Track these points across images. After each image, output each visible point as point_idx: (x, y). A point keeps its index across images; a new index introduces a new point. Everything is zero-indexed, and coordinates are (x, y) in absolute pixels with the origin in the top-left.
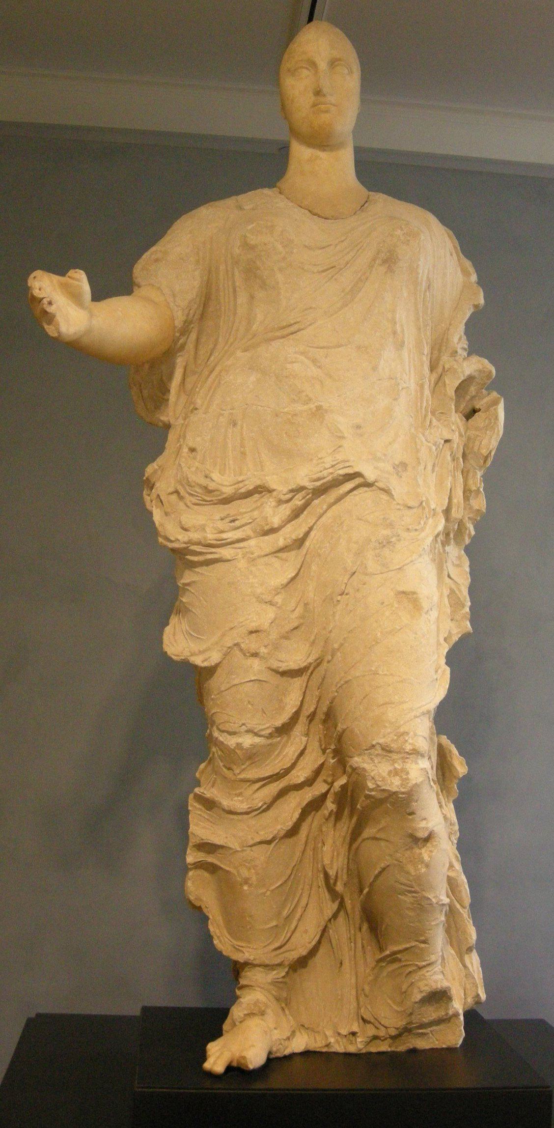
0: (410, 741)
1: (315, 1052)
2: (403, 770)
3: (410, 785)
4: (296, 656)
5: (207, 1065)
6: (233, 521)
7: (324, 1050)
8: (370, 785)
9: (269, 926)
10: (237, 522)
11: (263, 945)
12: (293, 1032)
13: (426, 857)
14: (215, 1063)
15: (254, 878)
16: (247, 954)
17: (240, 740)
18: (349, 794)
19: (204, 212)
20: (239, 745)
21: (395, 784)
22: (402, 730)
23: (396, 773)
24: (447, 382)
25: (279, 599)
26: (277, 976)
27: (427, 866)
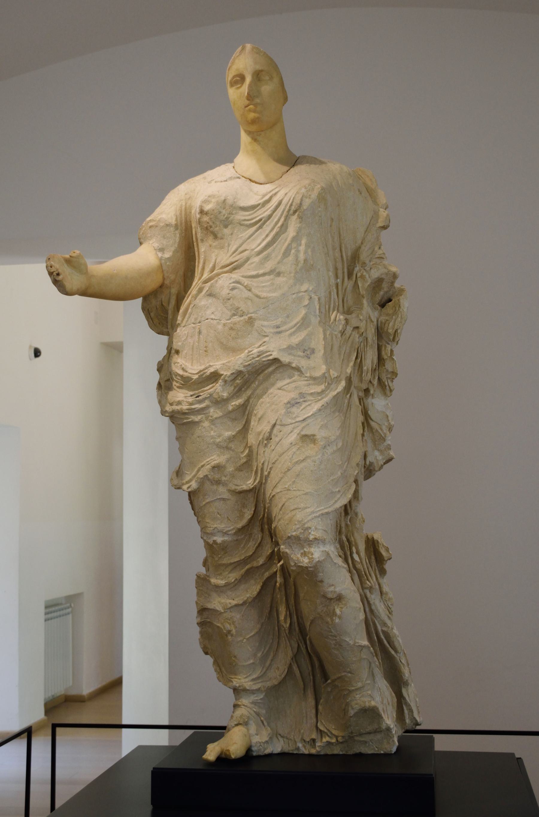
0: (313, 533)
2: (309, 552)
3: (314, 562)
4: (249, 483)
5: (204, 757)
7: (295, 752)
8: (293, 564)
10: (200, 398)
11: (245, 676)
12: (271, 738)
13: (338, 611)
14: (210, 754)
17: (215, 538)
20: (215, 542)
21: (305, 562)
22: (306, 526)
23: (304, 554)
25: (232, 445)
26: (256, 698)
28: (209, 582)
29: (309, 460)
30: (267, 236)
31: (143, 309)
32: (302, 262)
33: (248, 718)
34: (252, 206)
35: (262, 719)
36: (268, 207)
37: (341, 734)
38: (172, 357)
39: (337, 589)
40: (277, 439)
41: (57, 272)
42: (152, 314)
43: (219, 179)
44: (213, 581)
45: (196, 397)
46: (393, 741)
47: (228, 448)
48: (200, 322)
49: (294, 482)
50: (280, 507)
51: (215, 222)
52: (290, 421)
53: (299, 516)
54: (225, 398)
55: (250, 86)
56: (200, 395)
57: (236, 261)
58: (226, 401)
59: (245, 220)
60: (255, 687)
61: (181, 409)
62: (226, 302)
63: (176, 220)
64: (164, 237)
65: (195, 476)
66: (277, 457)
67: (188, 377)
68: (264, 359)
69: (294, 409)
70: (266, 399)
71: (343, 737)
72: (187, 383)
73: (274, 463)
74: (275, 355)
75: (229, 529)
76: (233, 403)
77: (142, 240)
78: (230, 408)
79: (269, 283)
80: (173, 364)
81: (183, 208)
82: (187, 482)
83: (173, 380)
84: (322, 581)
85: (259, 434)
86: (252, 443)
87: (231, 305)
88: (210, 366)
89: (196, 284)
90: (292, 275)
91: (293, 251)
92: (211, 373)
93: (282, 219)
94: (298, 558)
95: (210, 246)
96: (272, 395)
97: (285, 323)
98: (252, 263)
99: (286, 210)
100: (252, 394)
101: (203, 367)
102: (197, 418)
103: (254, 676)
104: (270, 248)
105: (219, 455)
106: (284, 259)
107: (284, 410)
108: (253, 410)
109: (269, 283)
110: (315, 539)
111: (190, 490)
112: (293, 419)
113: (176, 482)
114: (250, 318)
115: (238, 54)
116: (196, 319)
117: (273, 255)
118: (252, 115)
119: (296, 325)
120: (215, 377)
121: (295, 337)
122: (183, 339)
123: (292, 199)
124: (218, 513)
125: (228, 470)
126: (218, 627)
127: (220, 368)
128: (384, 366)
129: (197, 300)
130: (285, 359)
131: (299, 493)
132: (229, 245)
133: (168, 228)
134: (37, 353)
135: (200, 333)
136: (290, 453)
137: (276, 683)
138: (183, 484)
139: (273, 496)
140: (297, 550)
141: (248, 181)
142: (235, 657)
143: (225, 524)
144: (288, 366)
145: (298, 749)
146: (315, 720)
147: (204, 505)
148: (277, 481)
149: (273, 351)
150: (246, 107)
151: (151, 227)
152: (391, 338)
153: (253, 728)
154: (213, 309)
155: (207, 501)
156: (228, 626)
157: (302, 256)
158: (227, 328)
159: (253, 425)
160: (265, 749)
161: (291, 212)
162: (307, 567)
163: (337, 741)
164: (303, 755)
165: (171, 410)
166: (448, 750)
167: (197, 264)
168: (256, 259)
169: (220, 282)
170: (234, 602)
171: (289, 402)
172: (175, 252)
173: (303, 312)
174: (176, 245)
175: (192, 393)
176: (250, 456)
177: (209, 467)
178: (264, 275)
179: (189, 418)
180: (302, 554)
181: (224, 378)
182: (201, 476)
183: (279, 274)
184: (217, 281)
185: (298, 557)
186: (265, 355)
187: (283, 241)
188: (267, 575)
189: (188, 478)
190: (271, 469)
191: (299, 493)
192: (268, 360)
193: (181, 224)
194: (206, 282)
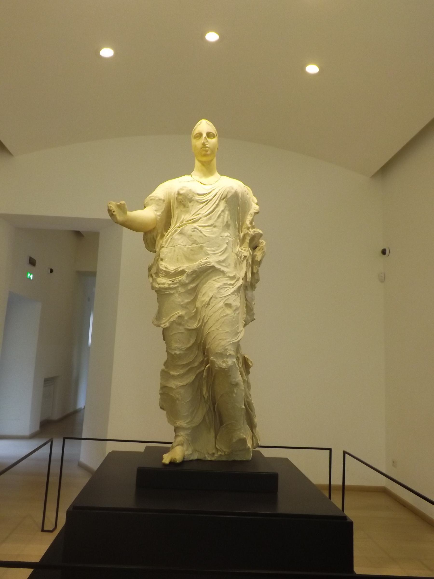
4: (195, 325)
5: (163, 461)
8: (217, 366)
12: (193, 452)
13: (235, 391)
17: (176, 352)
19: (185, 176)
20: (175, 354)
21: (224, 365)
22: (226, 348)
23: (224, 362)
25: (188, 306)
28: (169, 374)
31: (144, 239)
39: (236, 380)
40: (213, 305)
42: (148, 242)
44: (172, 373)
51: (184, 200)
52: (219, 296)
53: (223, 343)
60: (188, 427)
69: (222, 291)
70: (207, 285)
71: (228, 452)
72: (167, 274)
74: (213, 264)
77: (146, 206)
78: (189, 288)
82: (164, 323)
88: (180, 267)
91: (222, 217)
97: (217, 250)
100: (200, 282)
101: (176, 267)
102: (172, 292)
103: (187, 421)
110: (230, 355)
111: (165, 327)
113: (156, 323)
114: (201, 246)
116: (173, 244)
117: (213, 217)
120: (182, 272)
129: (174, 236)
130: (218, 266)
134: (51, 271)
135: (175, 251)
138: (161, 324)
143: (180, 346)
144: (218, 270)
145: (205, 457)
151: (151, 199)
153: (185, 446)
154: (182, 240)
155: (174, 333)
157: (226, 220)
161: (222, 198)
162: (224, 369)
168: (205, 219)
170: (182, 384)
171: (219, 287)
172: (162, 213)
173: (226, 245)
176: (197, 312)
177: (176, 316)
182: (172, 320)
183: (215, 227)
184: (185, 227)
185: (221, 363)
188: (198, 371)
189: (164, 321)
194: (178, 227)
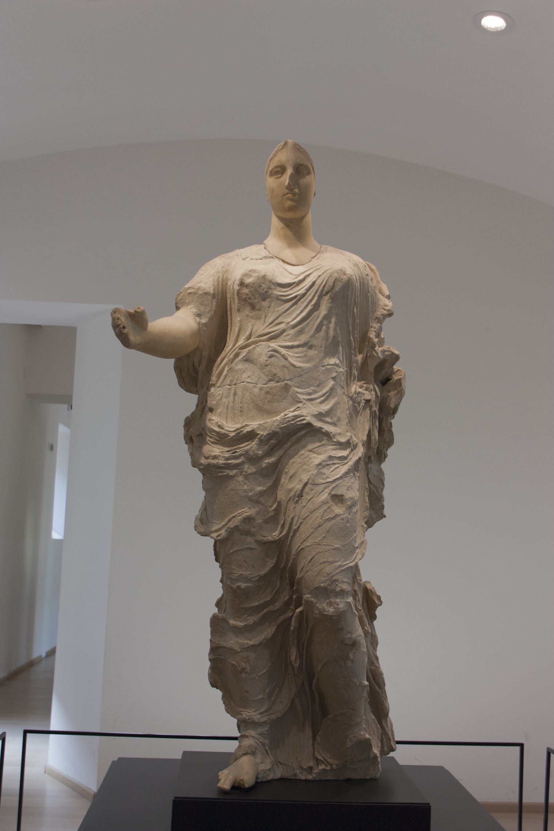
1: (287, 779)
2: (335, 603)
3: (340, 611)
4: (275, 535)
5: (219, 785)
6: (234, 453)
7: (292, 778)
9: (258, 698)
10: (236, 454)
13: (351, 656)
15: (248, 668)
16: (244, 716)
17: (239, 584)
18: (305, 616)
20: (239, 587)
22: (334, 578)
23: (330, 604)
24: (369, 363)
25: (262, 499)
26: (262, 730)
27: (352, 662)
28: (228, 623)
29: (338, 518)
30: (302, 312)
32: (331, 338)
33: (256, 748)
34: (289, 283)
35: (267, 748)
36: (304, 285)
37: (336, 762)
38: (206, 414)
40: (309, 497)
41: (123, 325)
43: (256, 257)
45: (233, 453)
46: (379, 768)
47: (258, 502)
48: (235, 385)
49: (324, 537)
50: (309, 560)
51: (258, 294)
52: (322, 481)
54: (260, 455)
55: (291, 177)
56: (237, 452)
57: (274, 332)
58: (259, 459)
59: (282, 296)
61: (217, 463)
62: (263, 368)
63: (214, 290)
64: (202, 304)
65: (225, 525)
66: (308, 513)
67: (224, 434)
68: (298, 423)
69: (325, 471)
70: (297, 459)
71: (337, 765)
72: (222, 439)
73: (305, 519)
74: (309, 419)
75: (253, 576)
76: (267, 461)
77: (179, 305)
78: (264, 465)
79: (303, 354)
80: (207, 421)
81: (221, 279)
82: (216, 531)
83: (207, 435)
84: (342, 629)
85: (290, 491)
86: (281, 499)
87: (269, 371)
89: (231, 349)
90: (323, 349)
91: (324, 328)
92: (248, 432)
93: (316, 298)
94: (324, 607)
95: (247, 316)
96: (304, 456)
97: (315, 392)
98: (288, 335)
99: (320, 290)
101: (238, 426)
102: (233, 472)
103: (262, 710)
104: (305, 323)
105: (250, 508)
106: (316, 334)
107: (316, 471)
108: (284, 469)
109: (303, 354)
112: (324, 479)
114: (286, 385)
115: (280, 148)
116: (231, 381)
117: (307, 329)
118: (289, 203)
119: (325, 394)
120: (251, 435)
121: (324, 405)
122: (218, 399)
123: (325, 281)
124: (245, 561)
125: (257, 522)
126: (233, 664)
127: (257, 428)
128: (383, 436)
131: (328, 548)
132: (266, 317)
133: (206, 296)
136: (321, 510)
137: (280, 716)
138: (212, 532)
139: (302, 549)
140: (322, 600)
141: (281, 263)
142: (247, 692)
145: (295, 775)
146: (312, 749)
147: (232, 553)
148: (308, 535)
149: (306, 416)
150: (284, 195)
151: (189, 294)
152: (391, 412)
154: (249, 373)
155: (236, 549)
156: (244, 664)
157: (331, 333)
158: (263, 392)
159: (283, 483)
160: (268, 775)
161: (324, 292)
162: (331, 616)
163: (331, 768)
164: (301, 780)
165: (206, 463)
166: (471, 793)
167: (229, 331)
168: (292, 332)
169: (258, 349)
170: (251, 643)
171: (320, 464)
172: (211, 319)
173: (331, 383)
174: (212, 313)
175: (228, 449)
176: (278, 510)
177: (240, 518)
178: (298, 346)
179: (225, 472)
180: (328, 603)
181: (261, 437)
182: (232, 526)
183: (311, 347)
186: (299, 419)
187: (316, 317)
190: (301, 524)
191: (328, 548)
192: (302, 424)
193: (218, 294)
194: (243, 348)
